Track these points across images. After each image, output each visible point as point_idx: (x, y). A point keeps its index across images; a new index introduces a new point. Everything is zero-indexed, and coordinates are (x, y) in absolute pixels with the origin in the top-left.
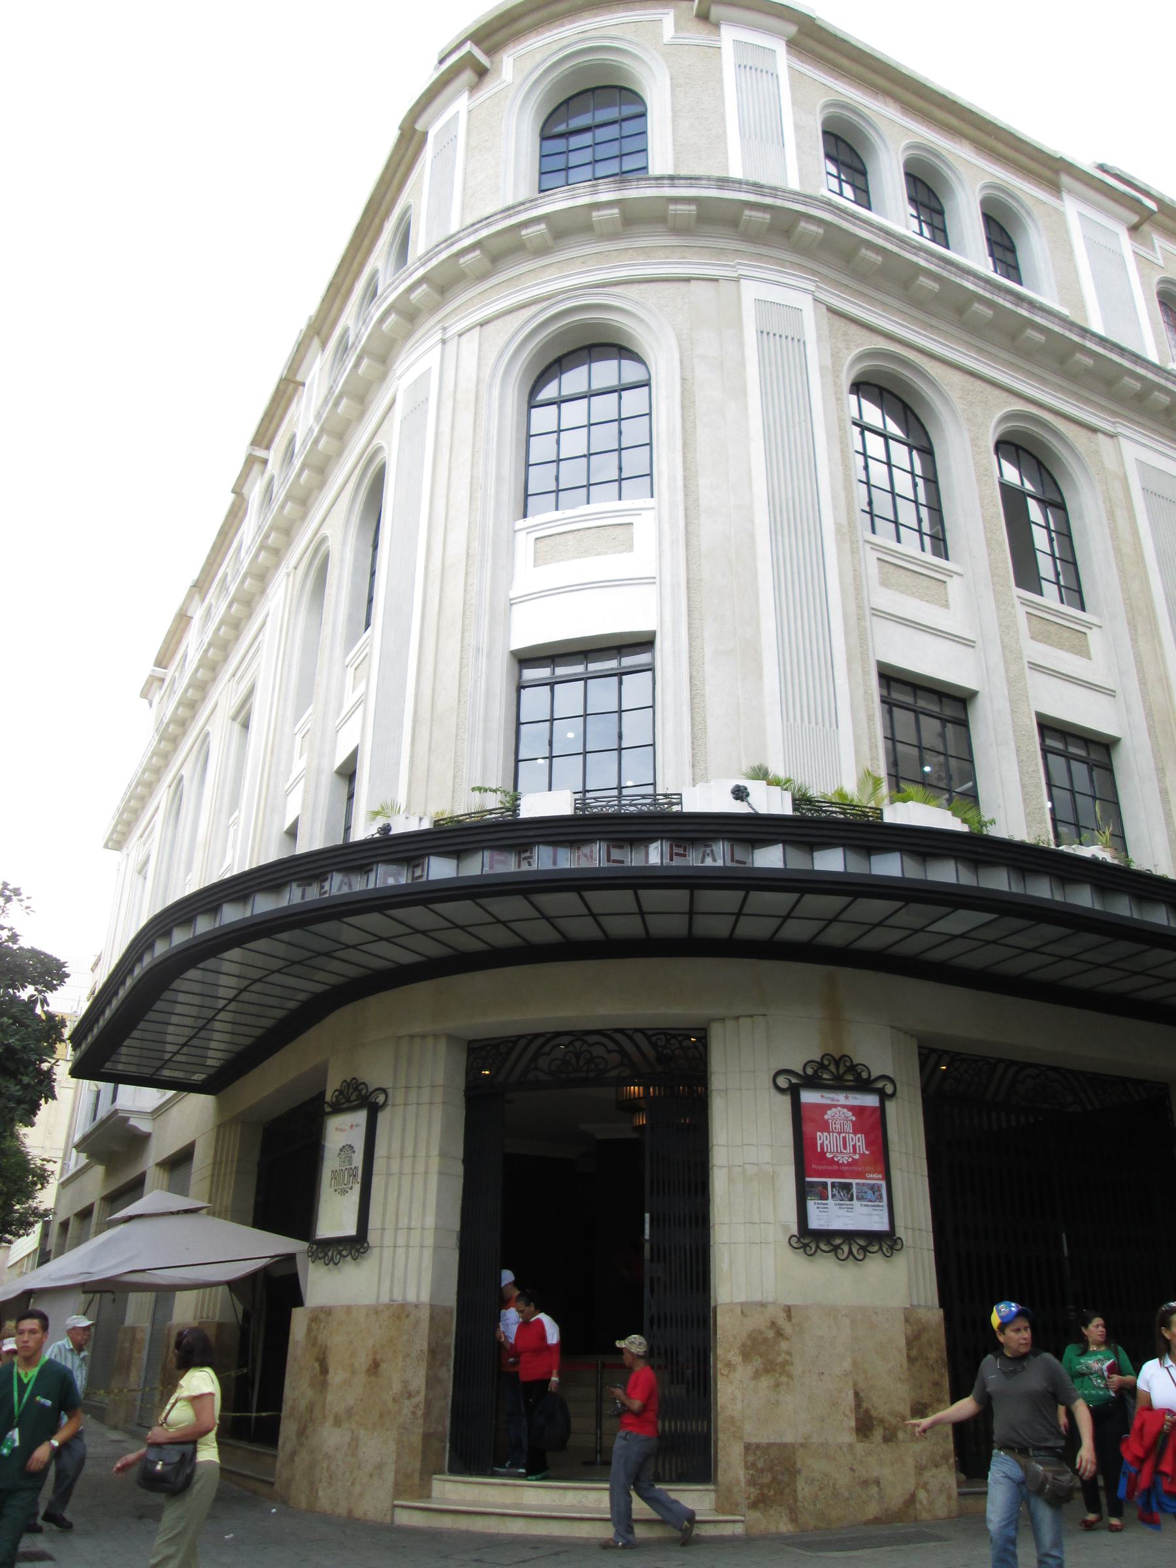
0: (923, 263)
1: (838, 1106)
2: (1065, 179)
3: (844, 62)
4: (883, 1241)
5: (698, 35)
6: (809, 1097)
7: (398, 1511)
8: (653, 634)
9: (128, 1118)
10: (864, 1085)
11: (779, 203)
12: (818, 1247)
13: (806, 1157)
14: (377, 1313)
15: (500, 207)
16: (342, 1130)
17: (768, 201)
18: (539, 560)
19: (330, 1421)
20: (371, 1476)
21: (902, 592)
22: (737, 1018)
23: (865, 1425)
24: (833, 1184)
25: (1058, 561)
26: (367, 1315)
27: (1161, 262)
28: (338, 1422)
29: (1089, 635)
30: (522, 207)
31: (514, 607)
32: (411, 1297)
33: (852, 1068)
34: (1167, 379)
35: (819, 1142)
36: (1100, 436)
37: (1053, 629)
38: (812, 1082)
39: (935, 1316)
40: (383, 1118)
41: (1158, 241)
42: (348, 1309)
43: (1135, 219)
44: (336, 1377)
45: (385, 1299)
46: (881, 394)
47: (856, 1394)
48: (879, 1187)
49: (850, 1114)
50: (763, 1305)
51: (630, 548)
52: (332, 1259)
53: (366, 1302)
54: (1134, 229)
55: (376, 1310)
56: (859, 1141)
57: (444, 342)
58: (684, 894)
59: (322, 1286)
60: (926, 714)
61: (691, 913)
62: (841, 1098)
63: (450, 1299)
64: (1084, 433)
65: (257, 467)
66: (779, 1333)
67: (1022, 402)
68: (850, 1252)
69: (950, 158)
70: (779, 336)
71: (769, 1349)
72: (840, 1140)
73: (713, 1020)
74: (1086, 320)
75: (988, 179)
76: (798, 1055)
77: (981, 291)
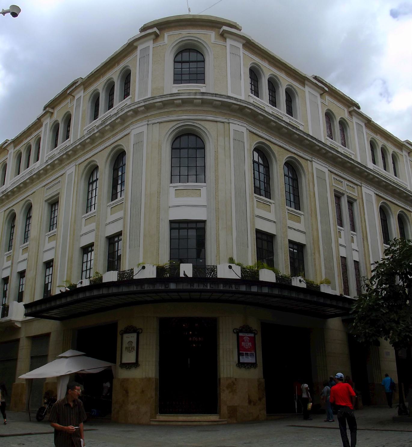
0: (273, 119)
1: (246, 336)
4: (253, 365)
5: (221, 42)
6: (241, 334)
9: (14, 323)
10: (251, 332)
11: (241, 104)
12: (242, 366)
15: (169, 93)
16: (129, 338)
18: (177, 196)
23: (250, 402)
24: (245, 353)
27: (327, 105)
28: (132, 404)
30: (175, 95)
32: (150, 376)
35: (242, 344)
36: (308, 161)
37: (293, 216)
39: (263, 380)
40: (141, 336)
42: (134, 379)
45: (144, 377)
47: (249, 396)
48: (254, 353)
49: (248, 338)
50: (230, 378)
52: (128, 368)
54: (321, 95)
56: (250, 344)
57: (76, 165)
58: (189, 226)
59: (123, 374)
60: (265, 242)
62: (247, 335)
63: (158, 377)
65: (48, 115)
66: (234, 384)
67: (291, 153)
68: (248, 367)
70: (239, 141)
71: (232, 386)
74: (309, 132)
76: (238, 325)
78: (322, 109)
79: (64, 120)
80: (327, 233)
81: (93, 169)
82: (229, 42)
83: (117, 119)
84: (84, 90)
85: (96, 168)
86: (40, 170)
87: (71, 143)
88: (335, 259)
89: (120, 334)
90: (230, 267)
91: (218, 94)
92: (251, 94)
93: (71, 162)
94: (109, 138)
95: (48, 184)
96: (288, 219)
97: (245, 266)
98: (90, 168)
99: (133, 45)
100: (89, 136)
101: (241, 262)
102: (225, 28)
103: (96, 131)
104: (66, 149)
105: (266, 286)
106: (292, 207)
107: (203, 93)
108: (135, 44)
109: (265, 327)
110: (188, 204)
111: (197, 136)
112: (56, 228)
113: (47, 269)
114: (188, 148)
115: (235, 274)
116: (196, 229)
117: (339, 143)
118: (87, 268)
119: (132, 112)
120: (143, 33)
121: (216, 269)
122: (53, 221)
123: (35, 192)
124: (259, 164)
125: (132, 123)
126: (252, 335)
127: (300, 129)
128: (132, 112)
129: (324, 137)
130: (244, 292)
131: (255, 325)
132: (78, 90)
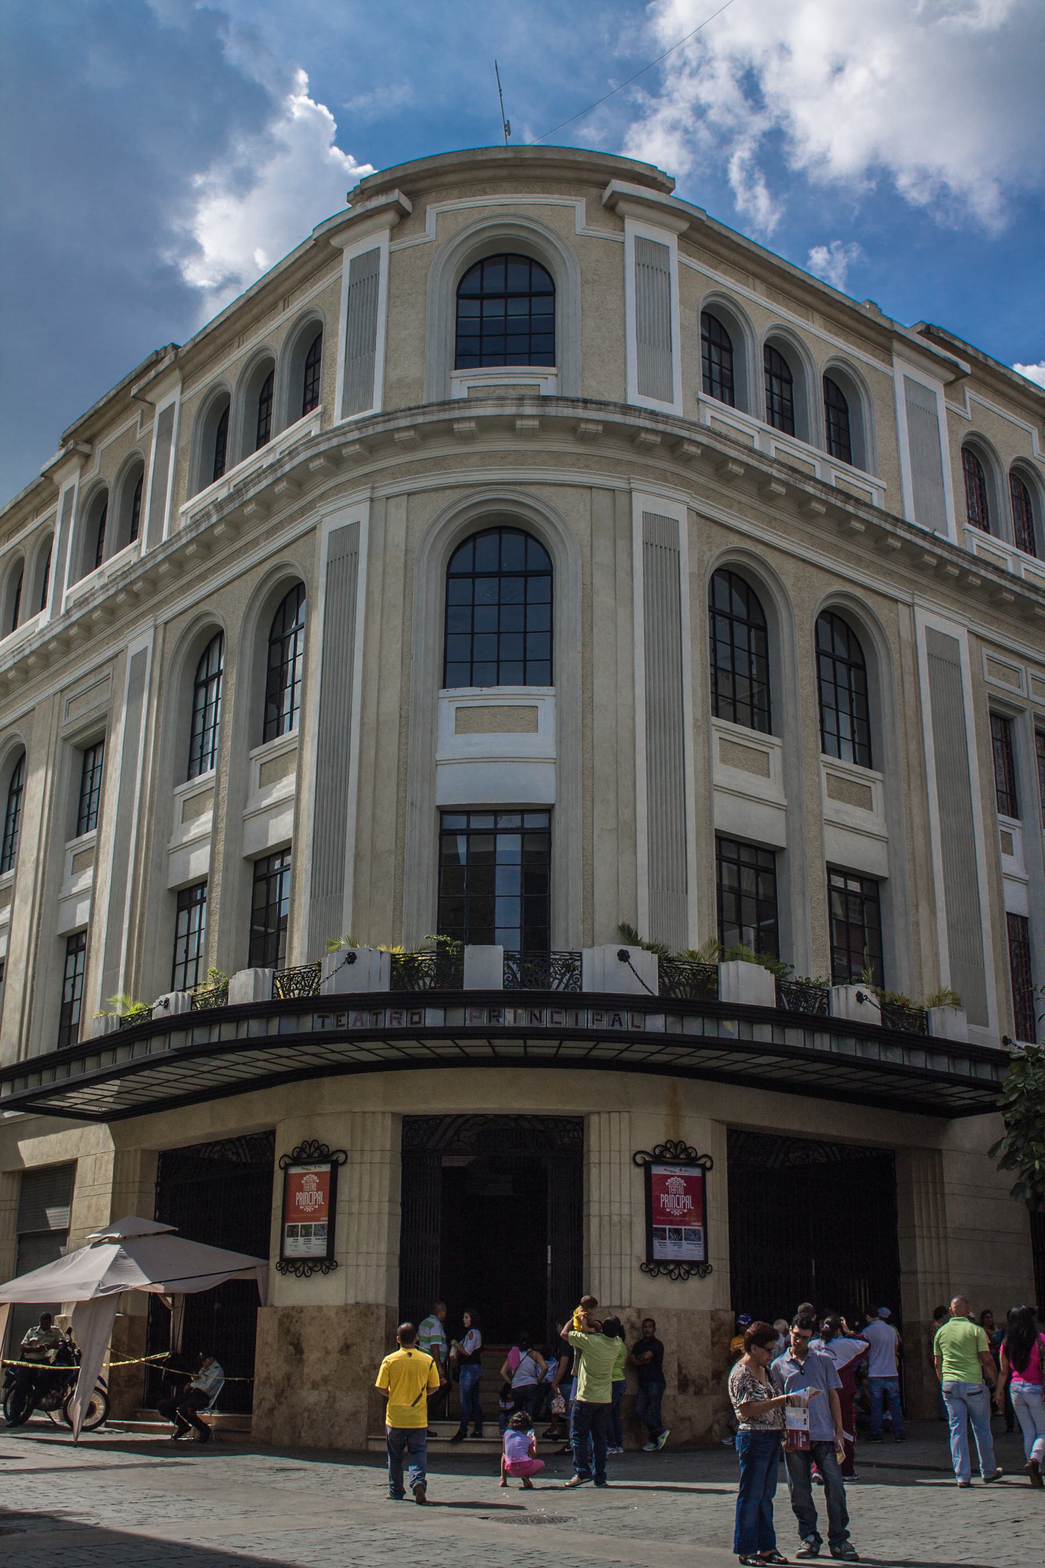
0: (775, 473)
1: (676, 1177)
2: (897, 346)
3: (724, 251)
5: (604, 231)
6: (658, 1170)
7: (370, 1442)
8: (553, 805)
10: (691, 1161)
11: (669, 429)
13: (653, 1210)
14: (346, 1311)
17: (661, 427)
19: (309, 1385)
20: (347, 1420)
21: (735, 766)
22: (609, 1112)
25: (854, 694)
26: (337, 1313)
27: (970, 417)
28: (315, 1386)
29: (873, 788)
31: (439, 767)
33: (685, 1150)
34: (958, 556)
36: (900, 606)
38: (658, 1159)
40: (344, 1172)
41: (970, 393)
42: (320, 1308)
43: (951, 377)
44: (312, 1356)
45: (351, 1301)
46: (730, 577)
47: (679, 1365)
51: (536, 729)
53: (337, 1304)
54: (948, 385)
55: (345, 1309)
56: (688, 1200)
57: (372, 500)
59: (287, 1292)
60: (750, 874)
61: (525, 1047)
62: (677, 1171)
64: (887, 603)
65: (75, 461)
69: (802, 336)
72: (675, 1201)
73: (593, 1113)
75: (833, 353)
76: (651, 1134)
77: (818, 494)
78: (951, 432)
79: (201, 420)
80: (959, 842)
81: (209, 641)
82: (634, 228)
83: (317, 456)
84: (183, 384)
85: (218, 635)
86: (48, 642)
87: (143, 554)
88: (986, 925)
89: (281, 1168)
90: (623, 956)
91: (591, 402)
92: (702, 395)
93: (143, 615)
94: (255, 543)
95: (83, 681)
96: (829, 796)
97: (673, 953)
98: (199, 637)
99: (329, 243)
100: (194, 534)
101: (661, 941)
102: (618, 185)
103: (214, 519)
104: (125, 574)
105: (730, 1018)
106: (843, 756)
107: (545, 400)
108: (335, 242)
109: (740, 1140)
110: (499, 748)
111: (528, 535)
112: (212, 768)
113: (181, 914)
114: (499, 574)
115: (643, 975)
116: (523, 834)
117: (1008, 543)
118: (187, 957)
119: (322, 460)
120: (359, 209)
121: (578, 963)
122: (200, 743)
123: (33, 709)
124: (731, 618)
125: (322, 496)
126: (696, 1172)
127: (875, 504)
128: (322, 460)
129: (959, 524)
130: (676, 1031)
131: (703, 1136)
132: (162, 387)
